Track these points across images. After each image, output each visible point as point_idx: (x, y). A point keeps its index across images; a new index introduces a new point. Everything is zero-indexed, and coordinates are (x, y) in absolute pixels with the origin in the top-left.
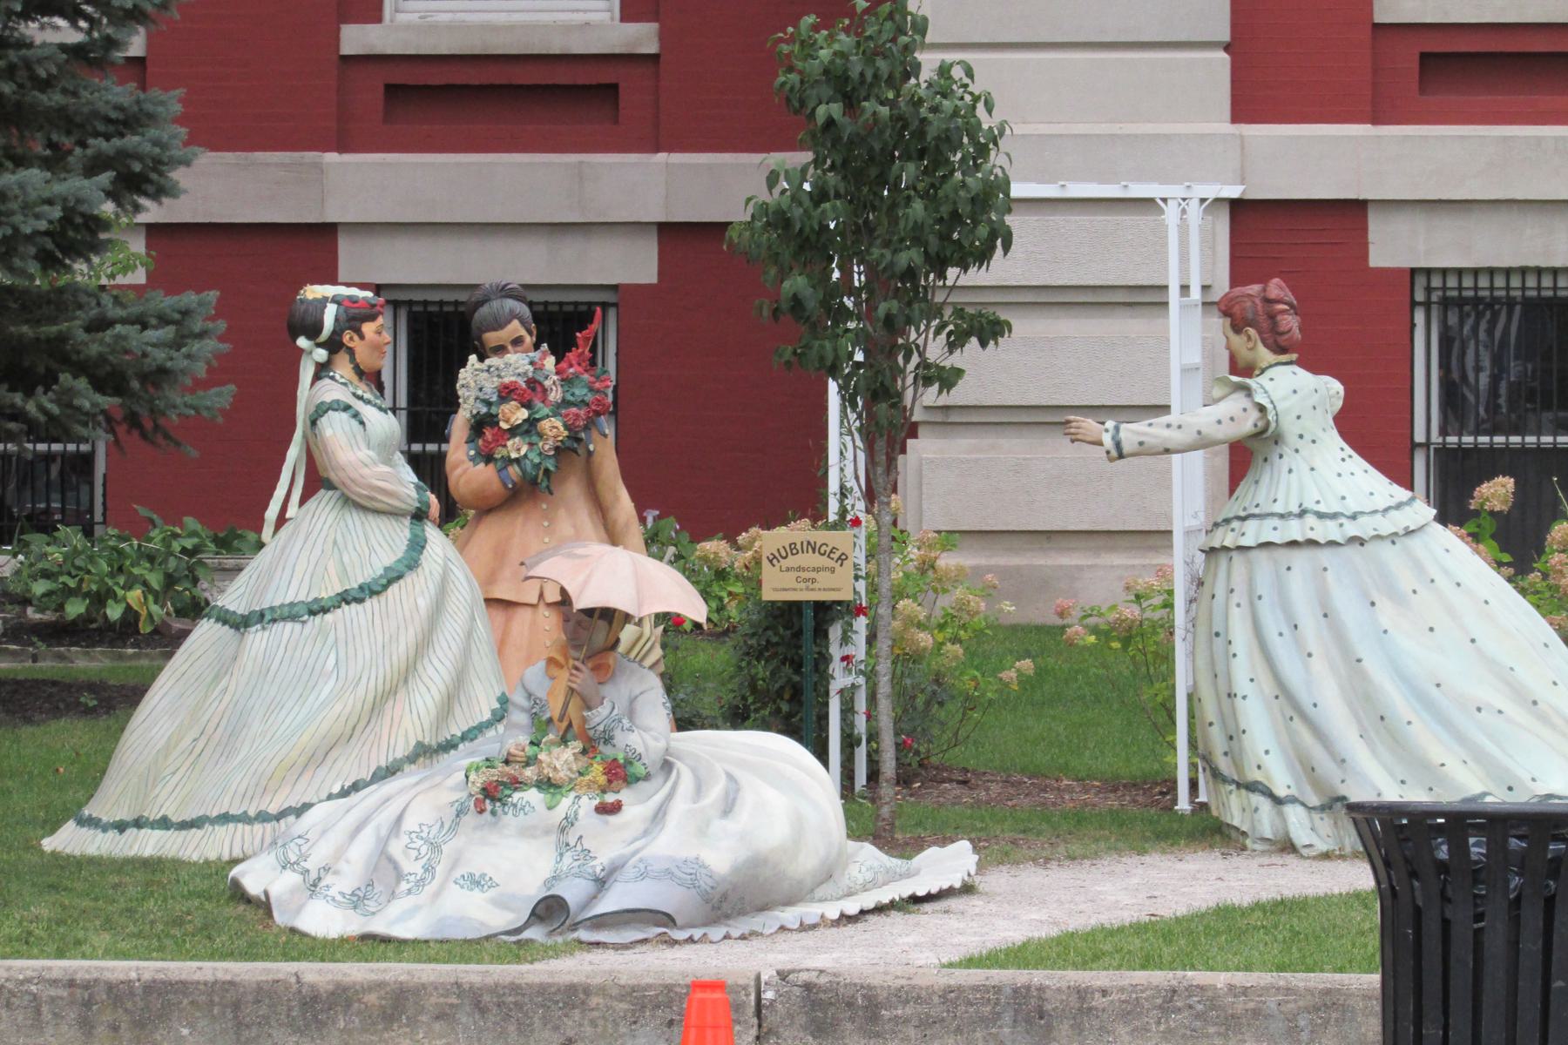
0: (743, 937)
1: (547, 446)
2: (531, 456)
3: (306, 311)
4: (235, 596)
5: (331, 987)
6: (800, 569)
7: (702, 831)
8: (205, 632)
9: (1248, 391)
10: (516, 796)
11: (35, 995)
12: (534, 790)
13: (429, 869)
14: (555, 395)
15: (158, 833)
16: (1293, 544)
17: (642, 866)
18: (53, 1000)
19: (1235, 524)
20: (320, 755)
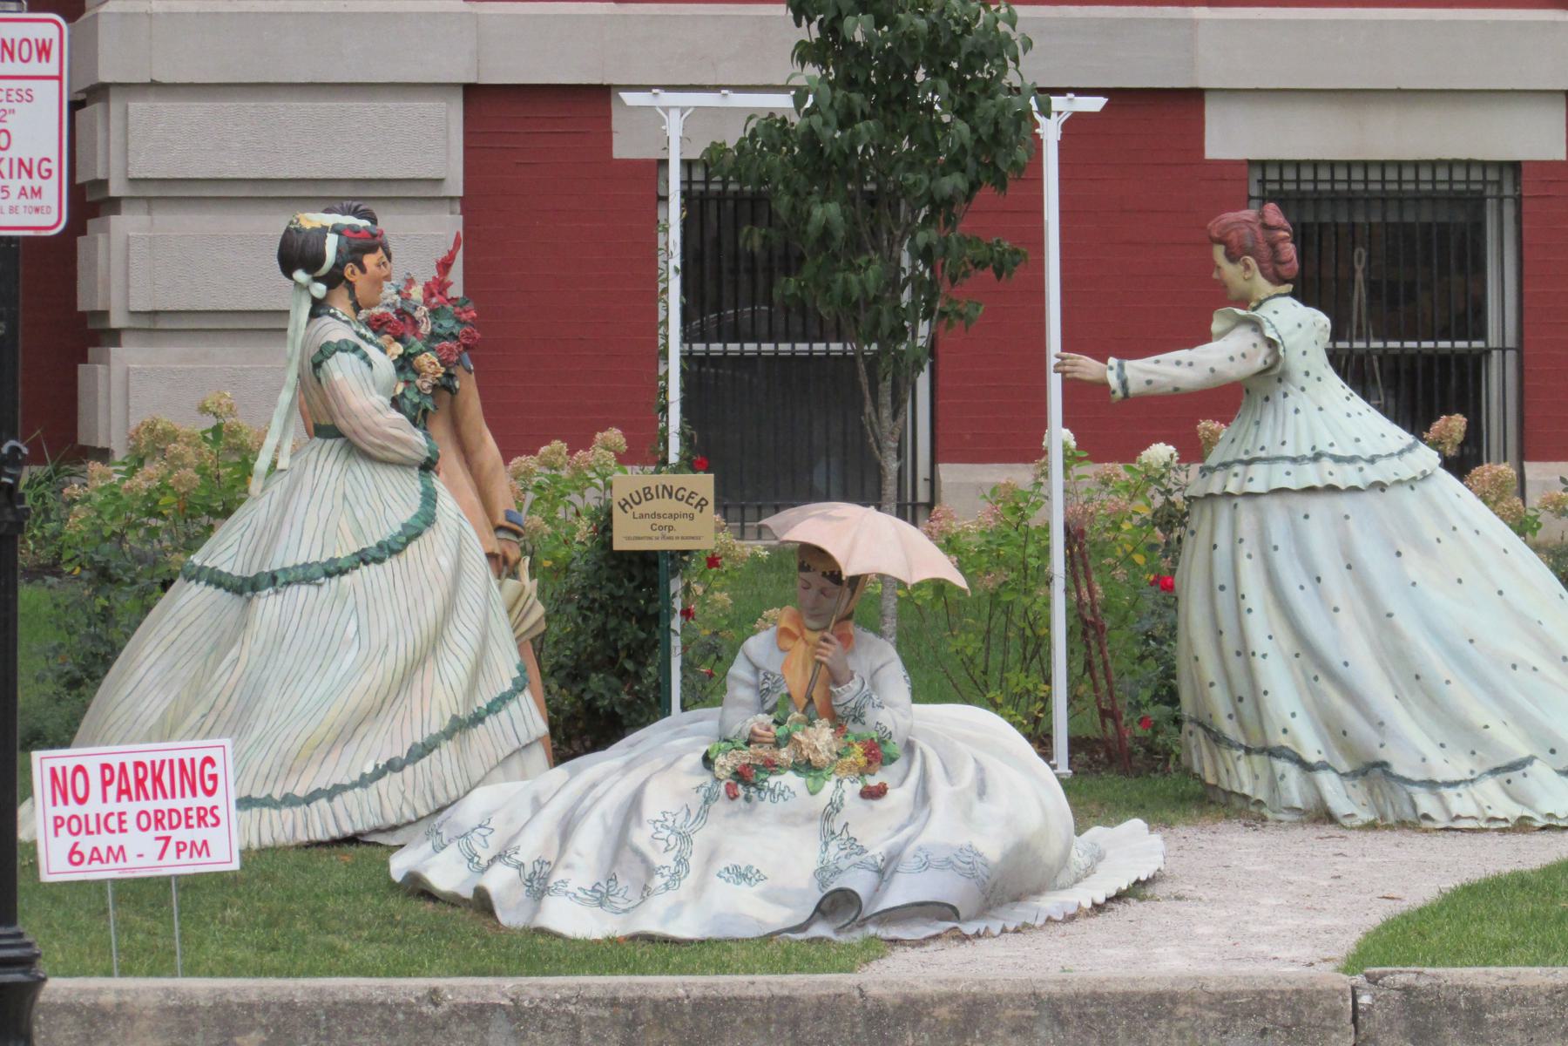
0: (1017, 931)
1: (425, 384)
2: (410, 395)
3: (305, 242)
4: (227, 550)
5: (898, 1001)
6: (656, 515)
7: (967, 816)
8: (189, 602)
9: (1256, 325)
11: (573, 1017)
13: (681, 861)
14: (426, 328)
16: (1311, 490)
17: (922, 855)
18: (593, 1020)
19: (1238, 469)
20: (348, 732)
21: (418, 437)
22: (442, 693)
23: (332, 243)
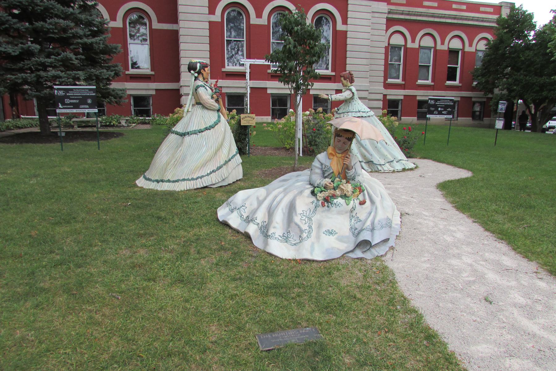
4: (179, 128)
8: (172, 137)
10: (335, 201)
12: (340, 198)
13: (310, 227)
15: (168, 183)
21: (217, 105)
22: (223, 156)
23: (198, 65)
